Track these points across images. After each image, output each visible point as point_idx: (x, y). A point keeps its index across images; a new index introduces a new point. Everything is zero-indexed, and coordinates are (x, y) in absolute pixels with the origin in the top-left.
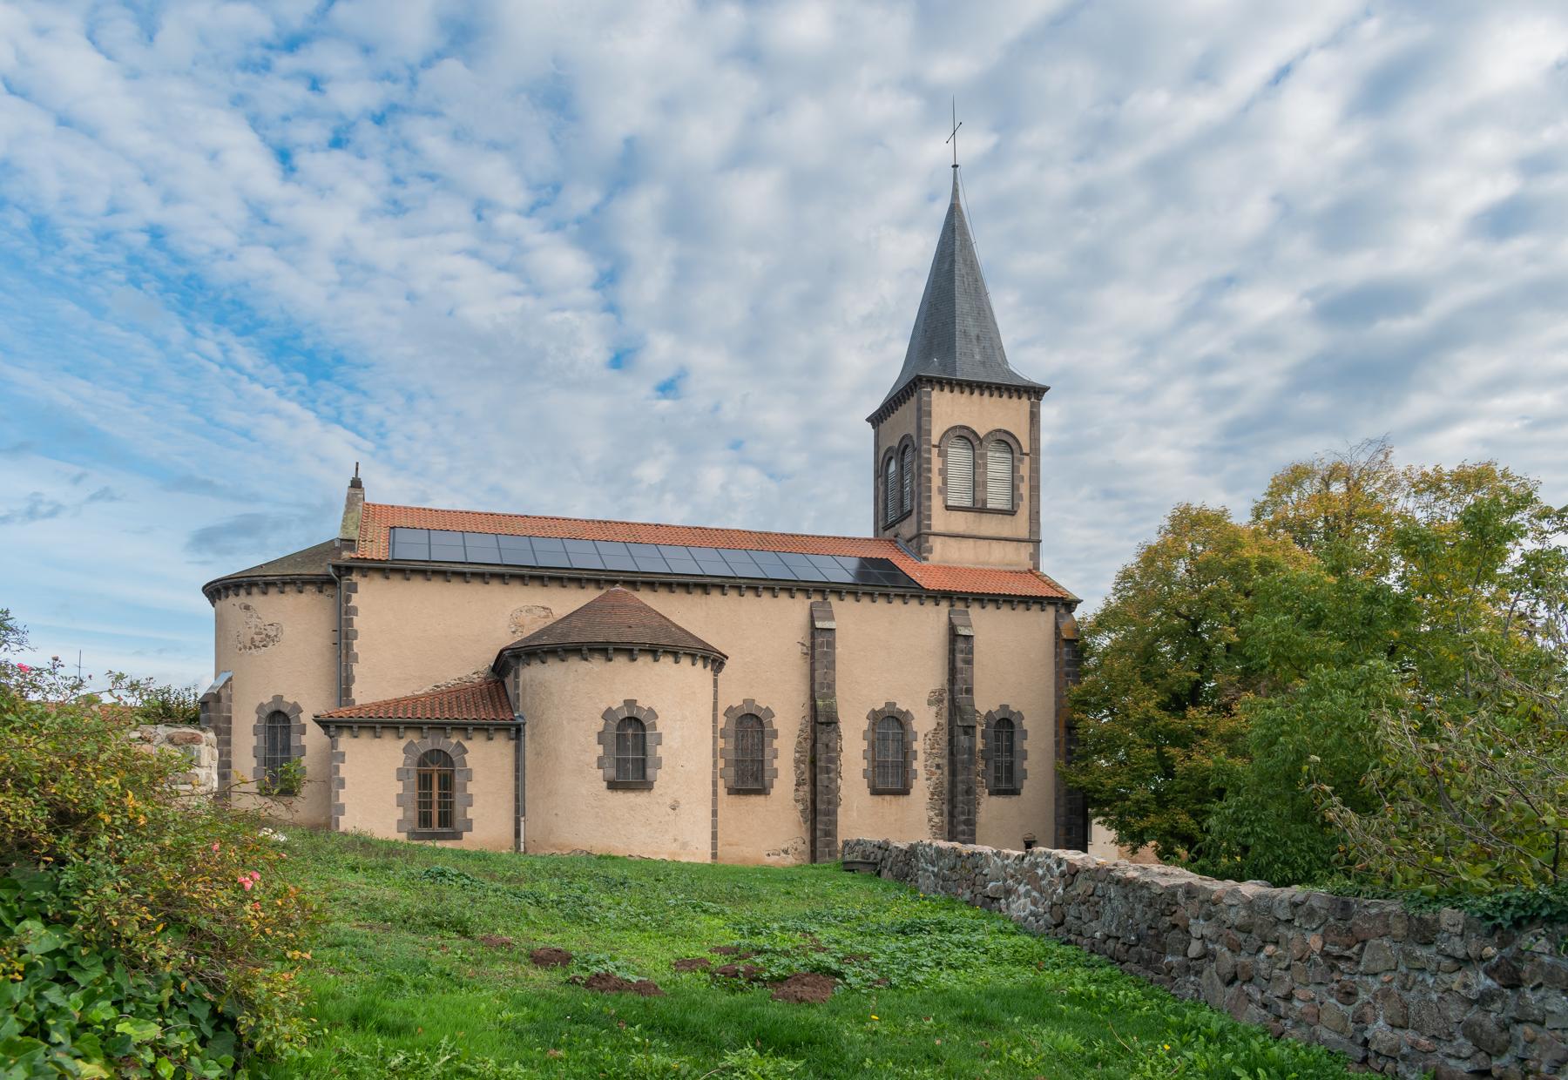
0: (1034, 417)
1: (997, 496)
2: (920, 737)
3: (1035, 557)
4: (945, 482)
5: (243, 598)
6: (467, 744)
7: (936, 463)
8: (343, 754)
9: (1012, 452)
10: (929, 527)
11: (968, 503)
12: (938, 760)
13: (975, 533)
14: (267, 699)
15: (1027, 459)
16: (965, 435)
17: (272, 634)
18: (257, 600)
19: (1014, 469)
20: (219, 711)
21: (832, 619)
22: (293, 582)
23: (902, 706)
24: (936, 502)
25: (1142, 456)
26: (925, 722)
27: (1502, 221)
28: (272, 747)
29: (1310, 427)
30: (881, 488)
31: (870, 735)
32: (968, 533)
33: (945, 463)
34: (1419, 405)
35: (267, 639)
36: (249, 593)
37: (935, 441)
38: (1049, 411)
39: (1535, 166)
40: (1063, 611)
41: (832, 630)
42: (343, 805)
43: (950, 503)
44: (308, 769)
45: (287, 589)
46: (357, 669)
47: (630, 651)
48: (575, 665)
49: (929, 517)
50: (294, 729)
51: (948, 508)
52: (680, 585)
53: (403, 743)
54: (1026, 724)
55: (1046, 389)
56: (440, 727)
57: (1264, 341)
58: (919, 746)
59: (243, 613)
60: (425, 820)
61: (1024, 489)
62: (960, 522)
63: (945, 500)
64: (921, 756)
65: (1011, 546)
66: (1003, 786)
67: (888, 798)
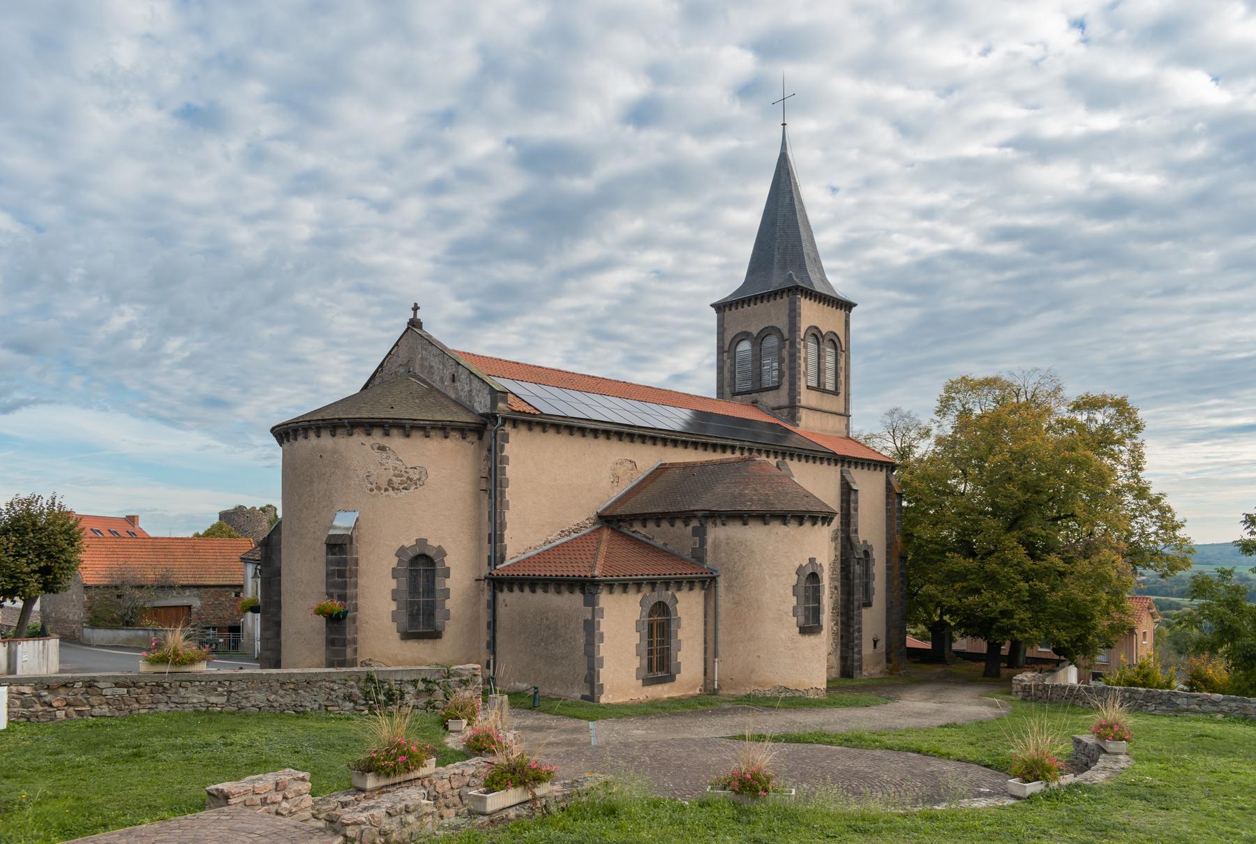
1: (830, 386)
3: (847, 426)
5: (377, 438)
6: (678, 595)
7: (803, 355)
9: (836, 348)
16: (816, 334)
17: (416, 477)
18: (396, 442)
25: (381, 259)
27: (642, 114)
28: (413, 590)
29: (514, 255)
34: (588, 250)
35: (407, 482)
36: (387, 434)
38: (857, 319)
39: (658, 73)
45: (432, 433)
46: (509, 516)
47: (784, 517)
48: (777, 528)
50: (438, 573)
53: (640, 596)
54: (449, 561)
56: (667, 584)
57: (473, 176)
59: (376, 454)
61: (842, 378)
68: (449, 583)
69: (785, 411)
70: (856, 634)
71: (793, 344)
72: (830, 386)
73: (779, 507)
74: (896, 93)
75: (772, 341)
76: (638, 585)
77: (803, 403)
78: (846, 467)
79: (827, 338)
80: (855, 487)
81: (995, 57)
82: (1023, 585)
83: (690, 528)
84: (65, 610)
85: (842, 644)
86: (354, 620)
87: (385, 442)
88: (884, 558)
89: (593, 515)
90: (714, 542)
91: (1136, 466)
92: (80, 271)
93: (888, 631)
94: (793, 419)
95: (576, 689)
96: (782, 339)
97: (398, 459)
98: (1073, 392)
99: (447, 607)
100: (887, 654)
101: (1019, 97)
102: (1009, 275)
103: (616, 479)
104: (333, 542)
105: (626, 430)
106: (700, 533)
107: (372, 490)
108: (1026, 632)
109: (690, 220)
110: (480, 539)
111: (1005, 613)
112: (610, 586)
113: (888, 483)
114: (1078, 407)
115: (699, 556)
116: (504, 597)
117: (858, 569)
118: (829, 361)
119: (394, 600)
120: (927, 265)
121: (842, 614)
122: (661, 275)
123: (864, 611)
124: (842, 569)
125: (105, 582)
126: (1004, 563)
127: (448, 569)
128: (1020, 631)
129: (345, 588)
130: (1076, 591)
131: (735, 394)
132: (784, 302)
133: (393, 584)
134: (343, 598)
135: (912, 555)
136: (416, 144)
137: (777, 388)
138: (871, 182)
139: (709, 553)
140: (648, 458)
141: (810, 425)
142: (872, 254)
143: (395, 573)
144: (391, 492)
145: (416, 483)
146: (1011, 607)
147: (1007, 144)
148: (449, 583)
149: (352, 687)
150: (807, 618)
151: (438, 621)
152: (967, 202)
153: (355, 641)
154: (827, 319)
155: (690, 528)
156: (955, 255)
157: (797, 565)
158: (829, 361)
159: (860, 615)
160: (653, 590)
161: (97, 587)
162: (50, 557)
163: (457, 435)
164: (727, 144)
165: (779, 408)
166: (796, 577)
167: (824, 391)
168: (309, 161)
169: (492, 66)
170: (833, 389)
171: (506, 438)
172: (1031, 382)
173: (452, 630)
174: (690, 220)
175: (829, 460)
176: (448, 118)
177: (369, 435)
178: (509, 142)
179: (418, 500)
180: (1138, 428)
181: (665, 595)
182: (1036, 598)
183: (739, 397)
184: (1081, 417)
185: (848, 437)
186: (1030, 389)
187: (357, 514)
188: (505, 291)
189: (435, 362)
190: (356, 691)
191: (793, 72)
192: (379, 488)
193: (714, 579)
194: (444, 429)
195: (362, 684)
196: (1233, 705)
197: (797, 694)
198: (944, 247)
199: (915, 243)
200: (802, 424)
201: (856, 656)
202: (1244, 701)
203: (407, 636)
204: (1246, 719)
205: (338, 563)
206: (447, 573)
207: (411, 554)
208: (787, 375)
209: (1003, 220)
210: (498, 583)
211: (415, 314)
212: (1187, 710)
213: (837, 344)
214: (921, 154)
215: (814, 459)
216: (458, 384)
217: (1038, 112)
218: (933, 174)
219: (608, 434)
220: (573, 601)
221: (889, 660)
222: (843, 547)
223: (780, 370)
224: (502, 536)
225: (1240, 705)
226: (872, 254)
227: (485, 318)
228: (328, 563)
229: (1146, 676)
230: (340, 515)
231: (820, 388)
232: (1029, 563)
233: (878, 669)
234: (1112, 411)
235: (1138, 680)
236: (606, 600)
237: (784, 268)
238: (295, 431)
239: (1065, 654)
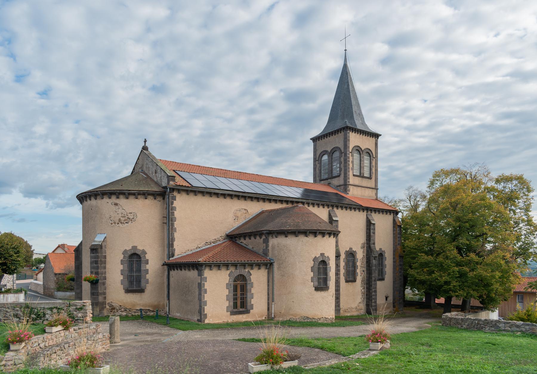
0: (376, 144)
1: (367, 174)
2: (359, 260)
3: (376, 194)
4: (353, 166)
5: (114, 199)
6: (251, 272)
7: (351, 159)
8: (206, 278)
9: (370, 156)
10: (349, 182)
11: (358, 174)
12: (364, 269)
13: (361, 185)
14: (129, 248)
16: (358, 150)
17: (131, 217)
18: (122, 201)
19: (371, 163)
20: (102, 253)
21: (337, 216)
22: (123, 194)
23: (354, 249)
24: (351, 174)
25: (229, 142)
26: (360, 255)
28: (131, 270)
31: (345, 260)
32: (359, 185)
33: (353, 159)
35: (128, 220)
36: (118, 198)
37: (350, 151)
41: (337, 221)
42: (206, 302)
44: (150, 280)
45: (139, 197)
46: (176, 235)
47: (305, 233)
48: (302, 239)
49: (349, 178)
51: (354, 175)
52: (249, 197)
53: (228, 272)
54: (148, 257)
55: (380, 135)
56: (244, 265)
57: (267, 105)
58: (359, 264)
59: (113, 207)
60: (235, 306)
63: (353, 172)
64: (359, 267)
66: (380, 277)
67: (350, 283)
68: (148, 267)
69: (342, 187)
70: (373, 293)
71: (346, 155)
72: (367, 174)
73: (303, 228)
74: (454, 57)
75: (337, 154)
76: (227, 266)
77: (351, 183)
78: (369, 212)
79: (365, 151)
80: (373, 222)
81: (501, 37)
82: (456, 269)
83: (262, 239)
84: (50, 284)
85: (367, 298)
86: (104, 284)
87: (117, 201)
88: (392, 257)
89: (224, 235)
90: (272, 246)
91: (527, 209)
92: (113, 153)
93: (394, 292)
94: (346, 191)
95: (195, 316)
96: (341, 153)
97: (123, 209)
98: (495, 175)
99: (147, 278)
100: (393, 303)
101: (513, 54)
102: (508, 134)
103: (236, 218)
104: (93, 248)
105: (241, 194)
106: (266, 242)
107: (112, 224)
108: (457, 292)
110: (164, 247)
111: (447, 283)
112: (210, 266)
113: (394, 220)
114: (498, 181)
115: (266, 253)
116: (173, 273)
117: (374, 262)
118: (366, 162)
119: (122, 274)
120: (469, 131)
121: (367, 284)
123: (378, 283)
124: (367, 262)
125: (63, 272)
126: (447, 258)
127: (148, 260)
128: (453, 291)
129: (98, 269)
130: (481, 271)
131: (321, 180)
132: (341, 135)
133: (121, 267)
134: (97, 273)
135: (404, 257)
136: (243, 94)
137: (339, 176)
138: (442, 97)
139: (270, 251)
140: (255, 208)
141: (354, 194)
142: (442, 128)
143: (122, 262)
144: (120, 225)
145: (132, 220)
146: (449, 280)
147: (507, 75)
148: (148, 267)
149: (17, 310)
150: (319, 283)
151: (143, 284)
152: (488, 103)
153: (104, 293)
154: (366, 143)
155: (262, 239)
156: (484, 127)
157: (314, 257)
158: (366, 162)
159: (376, 284)
160: (236, 269)
161: (60, 274)
162: (6, 259)
163: (152, 197)
164: (376, 84)
165: (339, 186)
166: (313, 262)
167: (363, 177)
168: (200, 104)
169: (275, 60)
170: (369, 176)
171: (174, 198)
172: (474, 169)
173: (149, 288)
175: (359, 209)
176: (257, 82)
177: (110, 198)
178: (281, 90)
179: (137, 227)
180: (529, 191)
181: (245, 271)
182: (462, 275)
183: (323, 182)
184: (500, 187)
185: (377, 199)
186: (473, 174)
187: (105, 235)
188: (279, 153)
189: (150, 165)
190: (19, 312)
191: (404, 52)
192: (115, 223)
193: (271, 264)
194: (145, 194)
195: (22, 309)
196: (527, 327)
197: (314, 320)
198: (477, 123)
199: (463, 122)
200: (351, 193)
201: (373, 304)
202: (533, 325)
203: (128, 291)
204: (533, 335)
205: (95, 258)
206: (147, 262)
207: (129, 253)
208: (343, 170)
209: (505, 110)
210: (171, 266)
211: (145, 144)
212: (504, 330)
213: (372, 155)
214: (465, 82)
215: (351, 208)
216: (157, 174)
217: (522, 60)
218: (470, 91)
219: (231, 196)
220: (192, 274)
221: (394, 307)
222: (367, 251)
223: (340, 168)
224: (172, 244)
225: (531, 327)
226: (442, 128)
227: (271, 164)
228: (91, 257)
229: (529, 315)
230: (98, 235)
231: (361, 176)
232: (459, 258)
233: (388, 311)
234: (515, 182)
235: (525, 317)
236: (207, 273)
237: (343, 119)
238: (86, 197)
239: (487, 303)
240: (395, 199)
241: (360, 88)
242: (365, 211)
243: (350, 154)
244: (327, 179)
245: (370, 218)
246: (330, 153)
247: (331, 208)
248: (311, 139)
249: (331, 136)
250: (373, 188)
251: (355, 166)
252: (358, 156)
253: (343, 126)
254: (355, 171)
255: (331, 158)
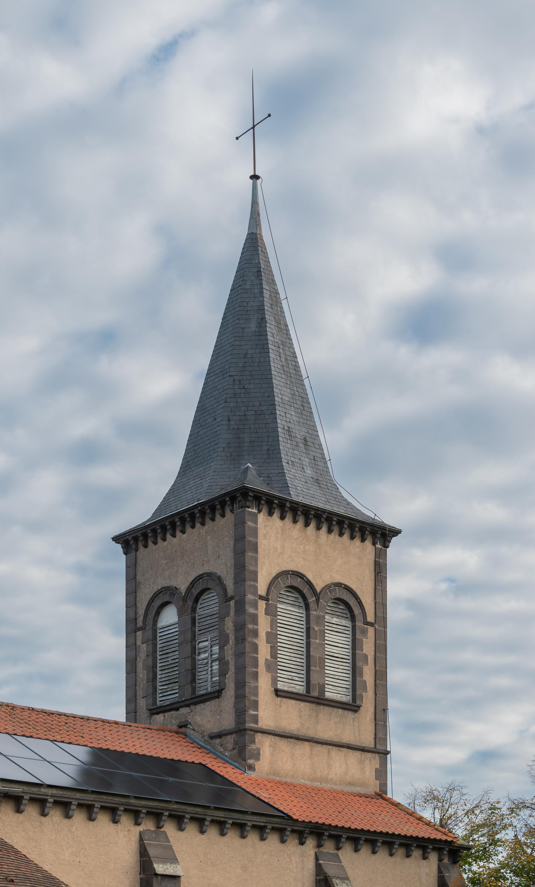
0: (380, 571)
1: (336, 689)
3: (381, 774)
4: (274, 654)
7: (264, 625)
9: (353, 618)
10: (255, 719)
11: (299, 688)
13: (311, 734)
15: (371, 631)
16: (296, 586)
21: (174, 860)
24: (264, 684)
27: (425, 322)
30: (144, 648)
37: (262, 590)
39: (456, 256)
40: (446, 861)
41: (175, 878)
43: (280, 686)
49: (255, 705)
51: (278, 693)
55: (396, 532)
61: (368, 675)
62: (292, 716)
63: (274, 681)
65: (354, 757)
75: (210, 605)
94: (242, 756)
109: (504, 494)
118: (336, 640)
122: (462, 587)
131: (155, 711)
132: (224, 524)
136: (55, 381)
137: (217, 694)
141: (279, 769)
158: (336, 640)
165: (220, 735)
167: (321, 701)
174: (504, 494)
175: (281, 832)
176: (106, 340)
183: (160, 718)
185: (381, 795)
213: (359, 613)
223: (221, 660)
231: (313, 697)
237: (236, 456)
240: (493, 799)
241: (326, 336)
242: (433, 857)
243: (262, 605)
244: (174, 707)
245: (330, 869)
246: (185, 599)
247: (148, 825)
248: (116, 539)
249: (189, 529)
250: (363, 750)
251: (282, 654)
252: (298, 612)
253: (229, 489)
254: (281, 674)
255: (188, 619)
